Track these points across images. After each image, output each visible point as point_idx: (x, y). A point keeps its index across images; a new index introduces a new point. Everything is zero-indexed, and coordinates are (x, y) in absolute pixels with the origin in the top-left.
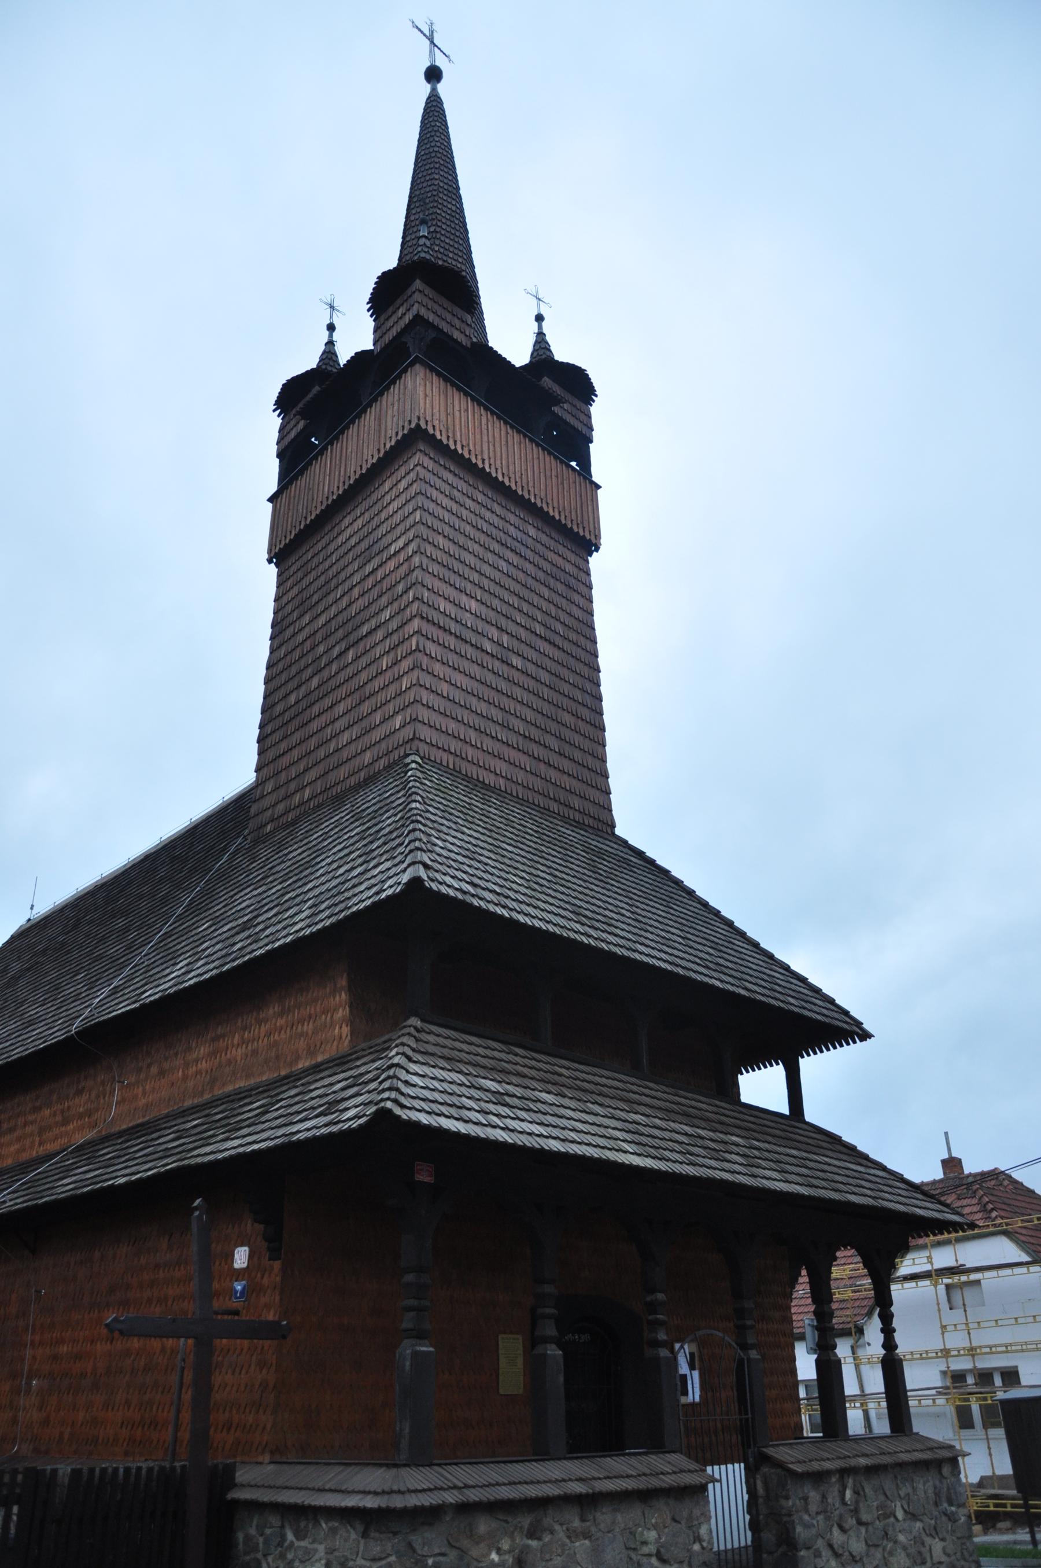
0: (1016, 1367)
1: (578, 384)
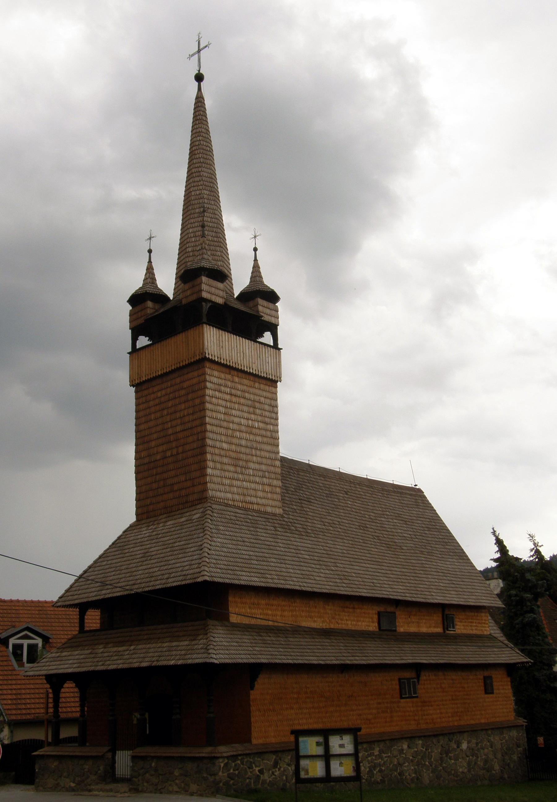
0: (128, 301)
1: (272, 297)
